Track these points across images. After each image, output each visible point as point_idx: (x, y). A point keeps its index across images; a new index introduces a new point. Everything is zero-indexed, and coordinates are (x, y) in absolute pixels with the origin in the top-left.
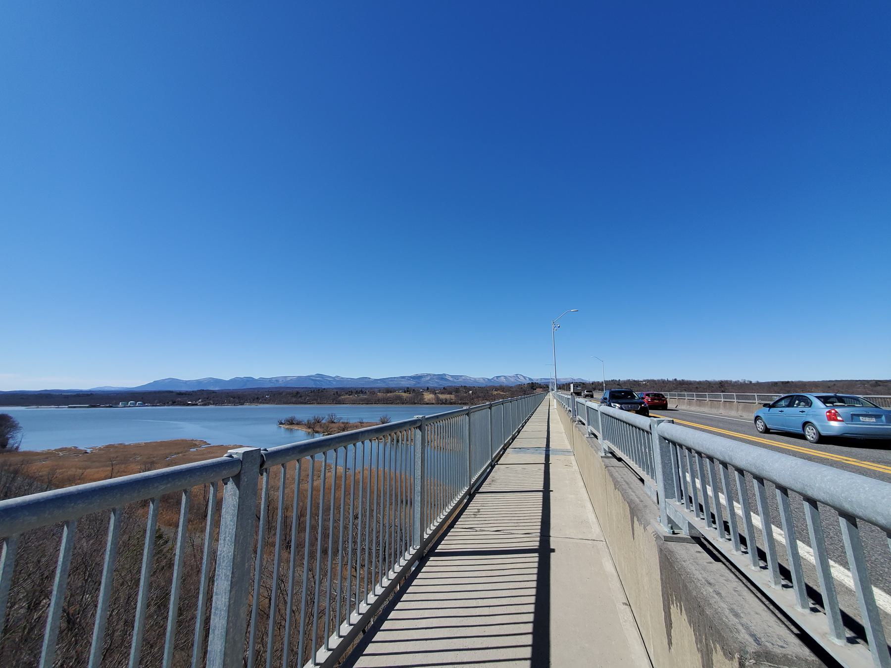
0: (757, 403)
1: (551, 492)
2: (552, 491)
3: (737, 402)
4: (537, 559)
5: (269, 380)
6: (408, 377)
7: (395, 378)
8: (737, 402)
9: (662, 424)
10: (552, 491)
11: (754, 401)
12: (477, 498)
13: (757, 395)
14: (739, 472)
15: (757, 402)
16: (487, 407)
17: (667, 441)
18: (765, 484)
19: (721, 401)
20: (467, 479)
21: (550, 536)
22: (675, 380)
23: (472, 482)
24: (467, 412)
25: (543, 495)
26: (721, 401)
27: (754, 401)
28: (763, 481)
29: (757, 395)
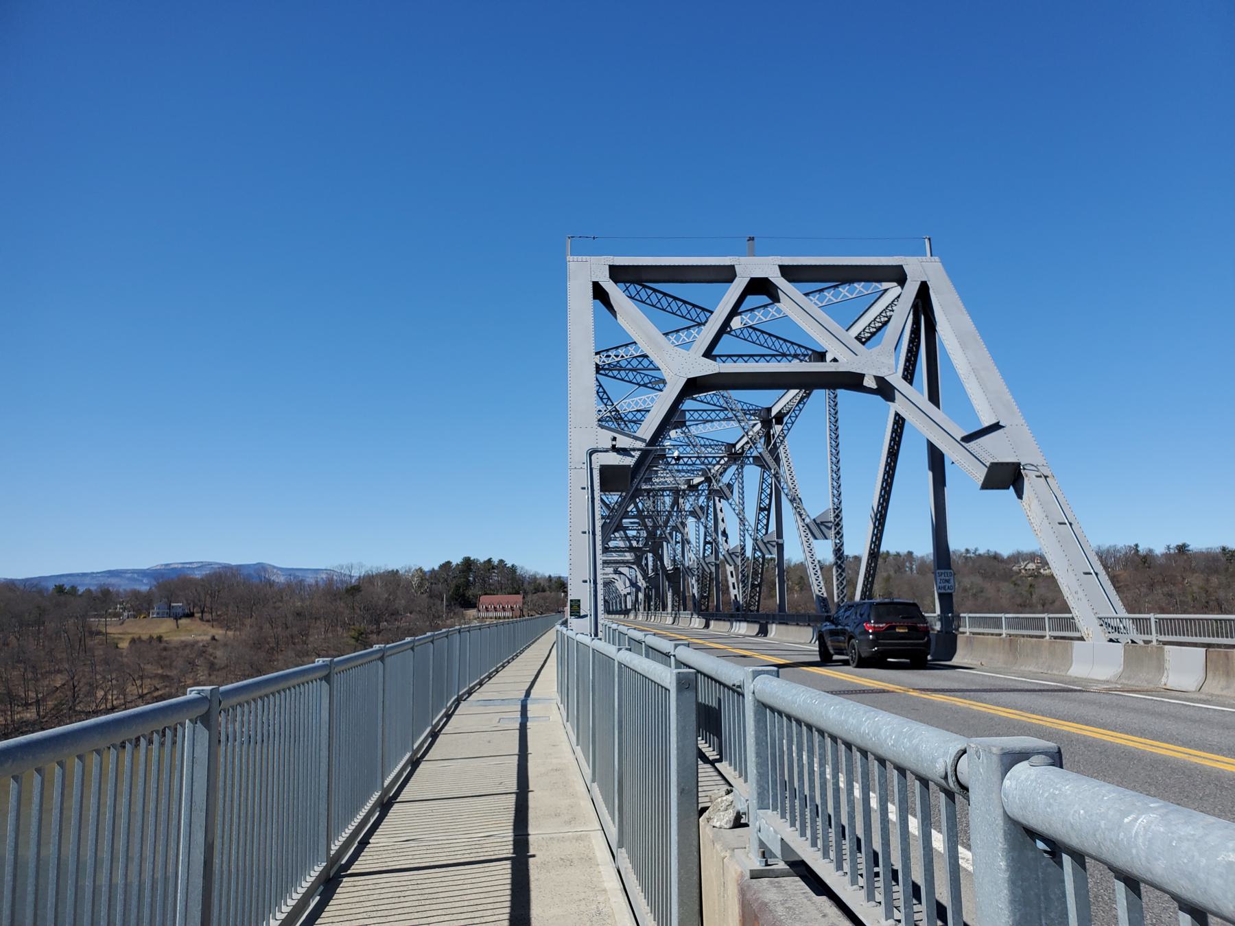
0: (1004, 635)
1: (531, 860)
2: (534, 856)
3: (1051, 637)
4: (509, 866)
5: (948, 808)
6: (134, 571)
7: (84, 575)
8: (1051, 637)
9: (1021, 768)
10: (534, 856)
11: (997, 631)
12: (378, 833)
13: (1049, 618)
14: (861, 753)
15: (1048, 633)
16: (427, 640)
17: (1041, 845)
18: (956, 800)
19: (1043, 637)
20: (322, 849)
21: (528, 835)
22: (1182, 549)
23: (332, 852)
24: (324, 673)
25: (512, 869)
26: (1043, 637)
27: (997, 631)
28: (954, 795)
29: (969, 617)
